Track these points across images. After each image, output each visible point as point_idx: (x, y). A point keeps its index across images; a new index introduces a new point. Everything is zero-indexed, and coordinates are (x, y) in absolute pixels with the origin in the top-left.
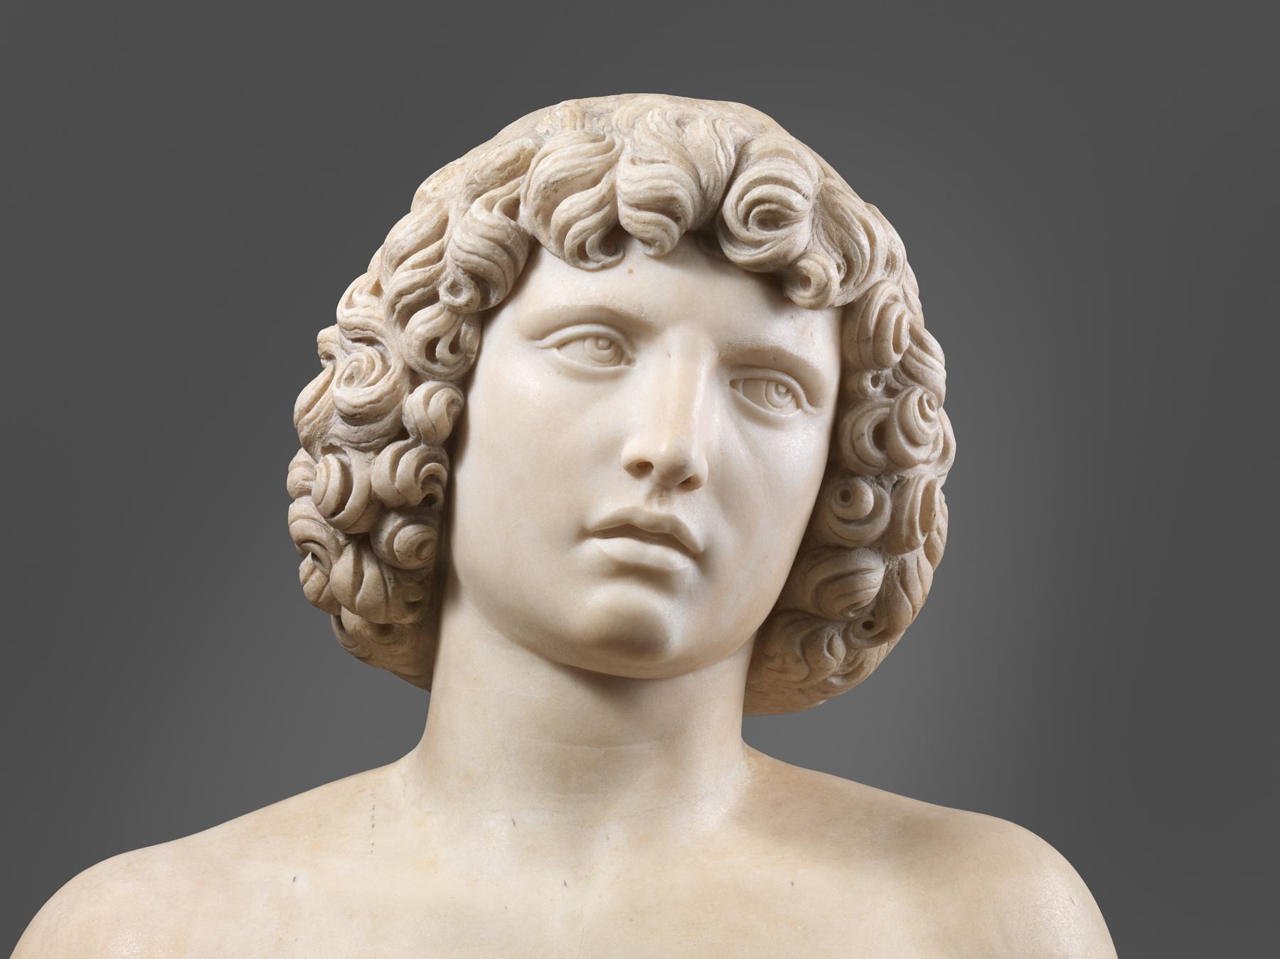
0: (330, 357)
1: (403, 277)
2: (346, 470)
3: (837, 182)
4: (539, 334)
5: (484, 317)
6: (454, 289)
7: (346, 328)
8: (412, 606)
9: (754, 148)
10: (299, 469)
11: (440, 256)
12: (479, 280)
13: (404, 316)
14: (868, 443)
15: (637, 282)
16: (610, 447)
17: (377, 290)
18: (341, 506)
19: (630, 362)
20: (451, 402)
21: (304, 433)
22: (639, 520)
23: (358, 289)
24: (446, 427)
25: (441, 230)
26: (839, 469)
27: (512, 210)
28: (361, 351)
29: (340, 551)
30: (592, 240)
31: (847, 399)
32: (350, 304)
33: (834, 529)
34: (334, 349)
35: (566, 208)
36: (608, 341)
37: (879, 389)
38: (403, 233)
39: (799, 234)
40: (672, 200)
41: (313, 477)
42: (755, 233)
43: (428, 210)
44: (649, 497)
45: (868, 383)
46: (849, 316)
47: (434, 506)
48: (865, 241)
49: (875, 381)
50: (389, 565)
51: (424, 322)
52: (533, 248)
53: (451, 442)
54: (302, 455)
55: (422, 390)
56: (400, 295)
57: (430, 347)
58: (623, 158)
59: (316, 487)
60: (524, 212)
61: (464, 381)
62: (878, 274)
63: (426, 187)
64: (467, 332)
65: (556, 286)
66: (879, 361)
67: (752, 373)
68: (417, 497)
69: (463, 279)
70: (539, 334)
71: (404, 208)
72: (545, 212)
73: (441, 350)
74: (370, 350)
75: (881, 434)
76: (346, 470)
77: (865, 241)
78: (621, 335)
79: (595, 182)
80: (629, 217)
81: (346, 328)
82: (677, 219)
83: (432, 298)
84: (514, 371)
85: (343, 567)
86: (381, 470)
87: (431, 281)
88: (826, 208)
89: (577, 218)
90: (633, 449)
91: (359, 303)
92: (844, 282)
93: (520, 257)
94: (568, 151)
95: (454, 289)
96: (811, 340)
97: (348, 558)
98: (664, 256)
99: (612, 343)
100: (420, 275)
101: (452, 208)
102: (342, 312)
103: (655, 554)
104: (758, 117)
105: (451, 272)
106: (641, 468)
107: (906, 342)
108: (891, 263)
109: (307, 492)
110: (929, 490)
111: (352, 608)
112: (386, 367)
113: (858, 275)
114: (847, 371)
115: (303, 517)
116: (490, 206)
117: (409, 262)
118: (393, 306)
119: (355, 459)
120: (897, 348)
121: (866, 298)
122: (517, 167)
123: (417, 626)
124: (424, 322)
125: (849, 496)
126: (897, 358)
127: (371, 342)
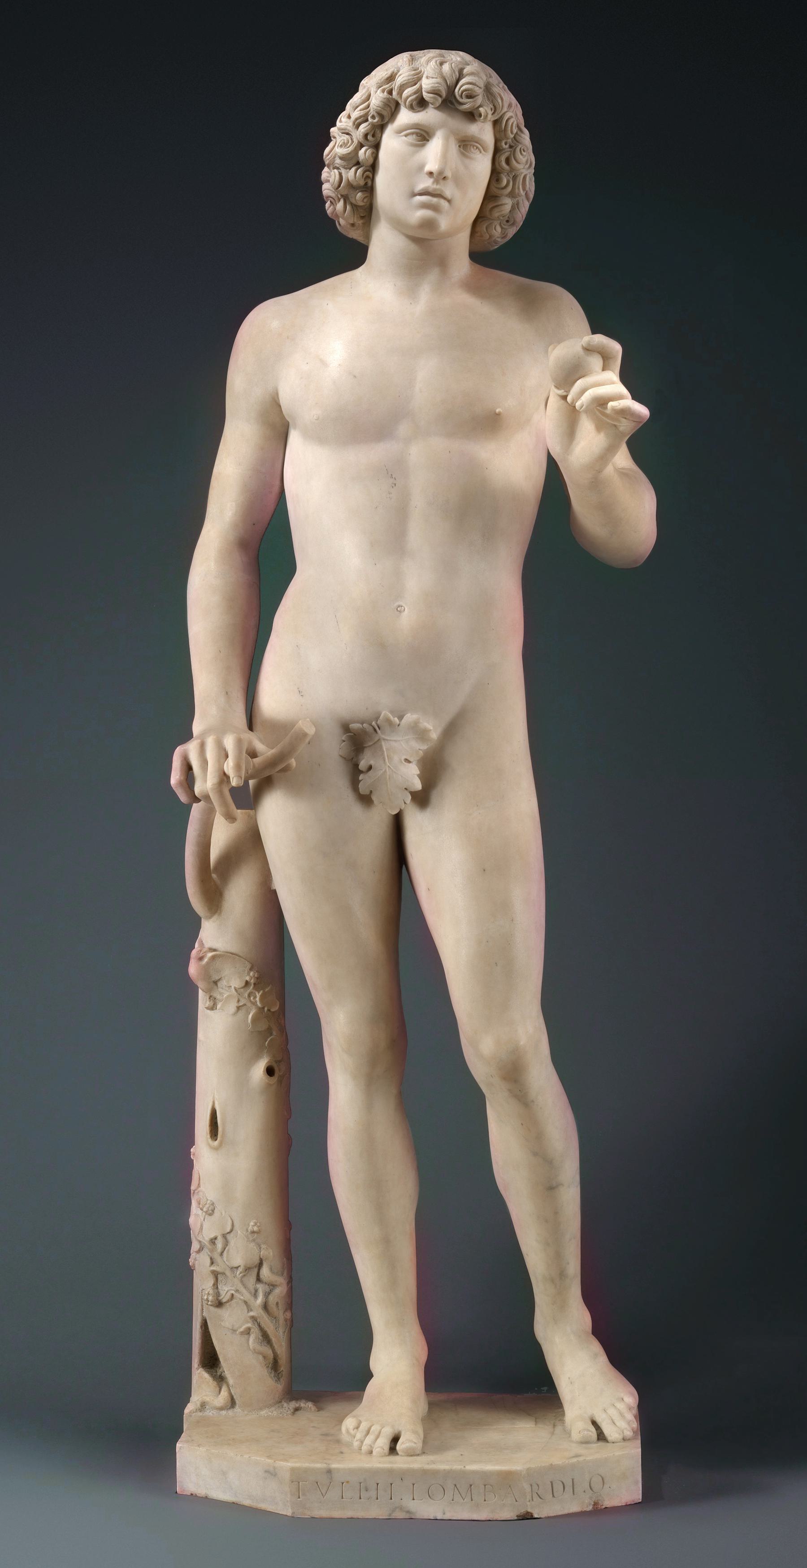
0: (335, 138)
1: (356, 114)
2: (340, 174)
3: (495, 79)
4: (399, 132)
5: (382, 127)
6: (373, 117)
7: (339, 129)
8: (362, 217)
9: (465, 71)
10: (325, 173)
11: (368, 106)
12: (381, 116)
13: (357, 127)
14: (503, 163)
15: (429, 116)
16: (421, 167)
17: (349, 117)
18: (339, 186)
19: (428, 141)
20: (373, 153)
21: (326, 163)
22: (430, 190)
23: (343, 117)
24: (371, 161)
25: (368, 97)
26: (495, 174)
27: (390, 92)
28: (344, 134)
29: (339, 200)
30: (414, 103)
31: (497, 151)
32: (341, 121)
33: (494, 190)
34: (336, 135)
35: (408, 92)
36: (419, 135)
37: (507, 146)
38: (357, 98)
39: (479, 100)
40: (439, 90)
41: (329, 177)
42: (464, 100)
43: (364, 91)
44: (433, 183)
45: (503, 144)
46: (496, 123)
47: (369, 188)
48: (500, 101)
49: (506, 144)
50: (355, 207)
51: (363, 128)
52: (397, 105)
53: (373, 167)
54: (326, 169)
55: (363, 149)
56: (356, 119)
57: (366, 136)
58: (424, 76)
59: (331, 180)
60: (394, 93)
61: (377, 147)
62: (505, 109)
63: (363, 82)
64: (378, 132)
65: (405, 117)
66: (506, 137)
67: (466, 144)
68: (362, 183)
69: (375, 114)
70: (399, 132)
71: (357, 90)
72: (400, 93)
73: (369, 137)
74: (347, 136)
75: (508, 161)
76: (340, 174)
77: (500, 101)
78: (423, 135)
79: (415, 84)
80: (426, 95)
81: (339, 129)
82: (441, 96)
83: (367, 120)
84: (392, 143)
85: (340, 205)
86: (350, 174)
87: (366, 115)
88: (488, 89)
89: (410, 96)
90: (428, 168)
91: (343, 121)
92: (493, 114)
93: (391, 108)
94: (407, 74)
95: (373, 117)
96: (484, 132)
97: (342, 202)
98: (437, 108)
99: (421, 135)
100: (363, 113)
101: (371, 88)
102: (338, 123)
103: (435, 200)
104: (468, 57)
105: (372, 112)
106: (431, 174)
107: (515, 131)
108: (510, 106)
109: (328, 181)
110: (525, 177)
111: (343, 218)
112: (353, 142)
113: (498, 111)
114: (497, 141)
115: (327, 189)
116: (383, 91)
117: (359, 108)
118: (354, 123)
119: (343, 171)
120: (512, 132)
121: (502, 117)
122: (391, 78)
123: (364, 224)
124: (363, 128)
125: (498, 180)
126: (512, 136)
127: (348, 134)
